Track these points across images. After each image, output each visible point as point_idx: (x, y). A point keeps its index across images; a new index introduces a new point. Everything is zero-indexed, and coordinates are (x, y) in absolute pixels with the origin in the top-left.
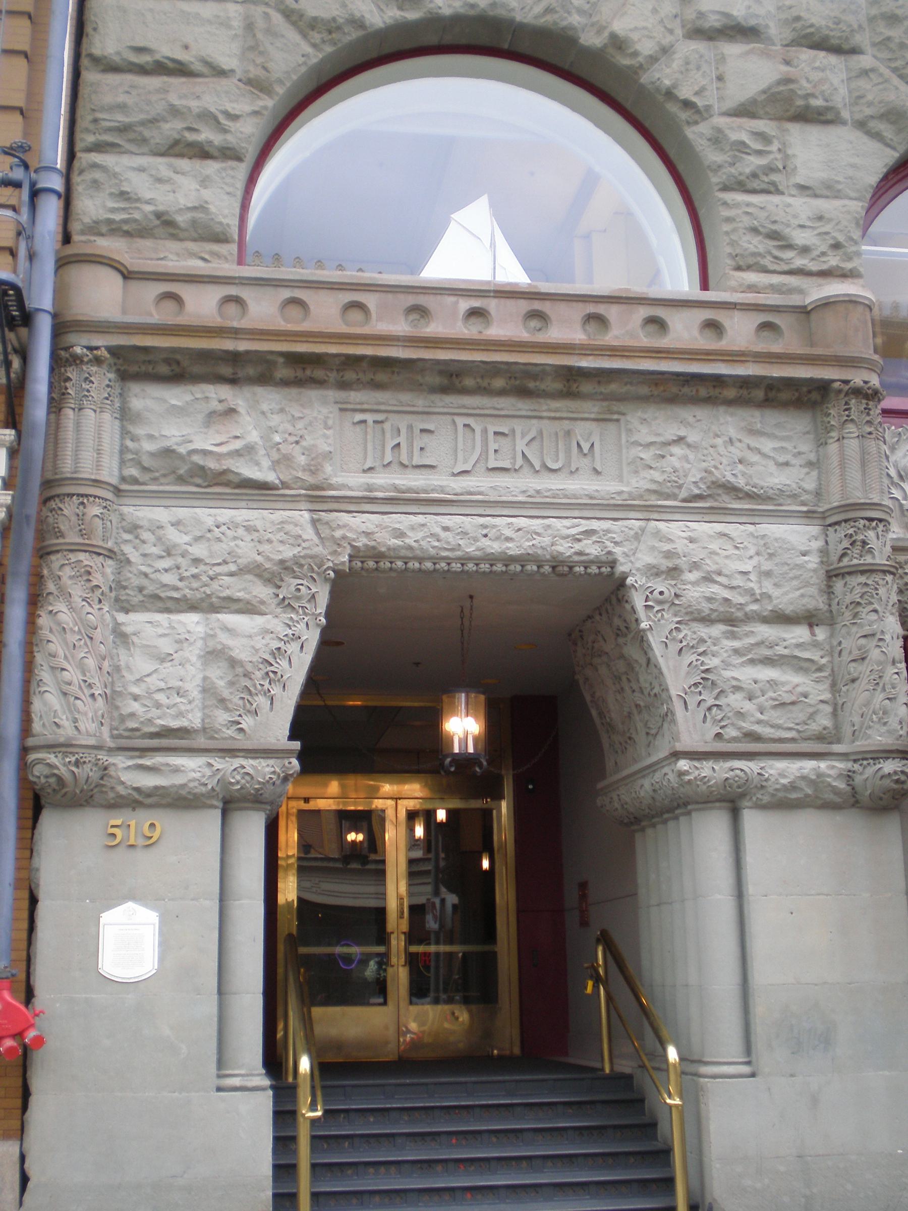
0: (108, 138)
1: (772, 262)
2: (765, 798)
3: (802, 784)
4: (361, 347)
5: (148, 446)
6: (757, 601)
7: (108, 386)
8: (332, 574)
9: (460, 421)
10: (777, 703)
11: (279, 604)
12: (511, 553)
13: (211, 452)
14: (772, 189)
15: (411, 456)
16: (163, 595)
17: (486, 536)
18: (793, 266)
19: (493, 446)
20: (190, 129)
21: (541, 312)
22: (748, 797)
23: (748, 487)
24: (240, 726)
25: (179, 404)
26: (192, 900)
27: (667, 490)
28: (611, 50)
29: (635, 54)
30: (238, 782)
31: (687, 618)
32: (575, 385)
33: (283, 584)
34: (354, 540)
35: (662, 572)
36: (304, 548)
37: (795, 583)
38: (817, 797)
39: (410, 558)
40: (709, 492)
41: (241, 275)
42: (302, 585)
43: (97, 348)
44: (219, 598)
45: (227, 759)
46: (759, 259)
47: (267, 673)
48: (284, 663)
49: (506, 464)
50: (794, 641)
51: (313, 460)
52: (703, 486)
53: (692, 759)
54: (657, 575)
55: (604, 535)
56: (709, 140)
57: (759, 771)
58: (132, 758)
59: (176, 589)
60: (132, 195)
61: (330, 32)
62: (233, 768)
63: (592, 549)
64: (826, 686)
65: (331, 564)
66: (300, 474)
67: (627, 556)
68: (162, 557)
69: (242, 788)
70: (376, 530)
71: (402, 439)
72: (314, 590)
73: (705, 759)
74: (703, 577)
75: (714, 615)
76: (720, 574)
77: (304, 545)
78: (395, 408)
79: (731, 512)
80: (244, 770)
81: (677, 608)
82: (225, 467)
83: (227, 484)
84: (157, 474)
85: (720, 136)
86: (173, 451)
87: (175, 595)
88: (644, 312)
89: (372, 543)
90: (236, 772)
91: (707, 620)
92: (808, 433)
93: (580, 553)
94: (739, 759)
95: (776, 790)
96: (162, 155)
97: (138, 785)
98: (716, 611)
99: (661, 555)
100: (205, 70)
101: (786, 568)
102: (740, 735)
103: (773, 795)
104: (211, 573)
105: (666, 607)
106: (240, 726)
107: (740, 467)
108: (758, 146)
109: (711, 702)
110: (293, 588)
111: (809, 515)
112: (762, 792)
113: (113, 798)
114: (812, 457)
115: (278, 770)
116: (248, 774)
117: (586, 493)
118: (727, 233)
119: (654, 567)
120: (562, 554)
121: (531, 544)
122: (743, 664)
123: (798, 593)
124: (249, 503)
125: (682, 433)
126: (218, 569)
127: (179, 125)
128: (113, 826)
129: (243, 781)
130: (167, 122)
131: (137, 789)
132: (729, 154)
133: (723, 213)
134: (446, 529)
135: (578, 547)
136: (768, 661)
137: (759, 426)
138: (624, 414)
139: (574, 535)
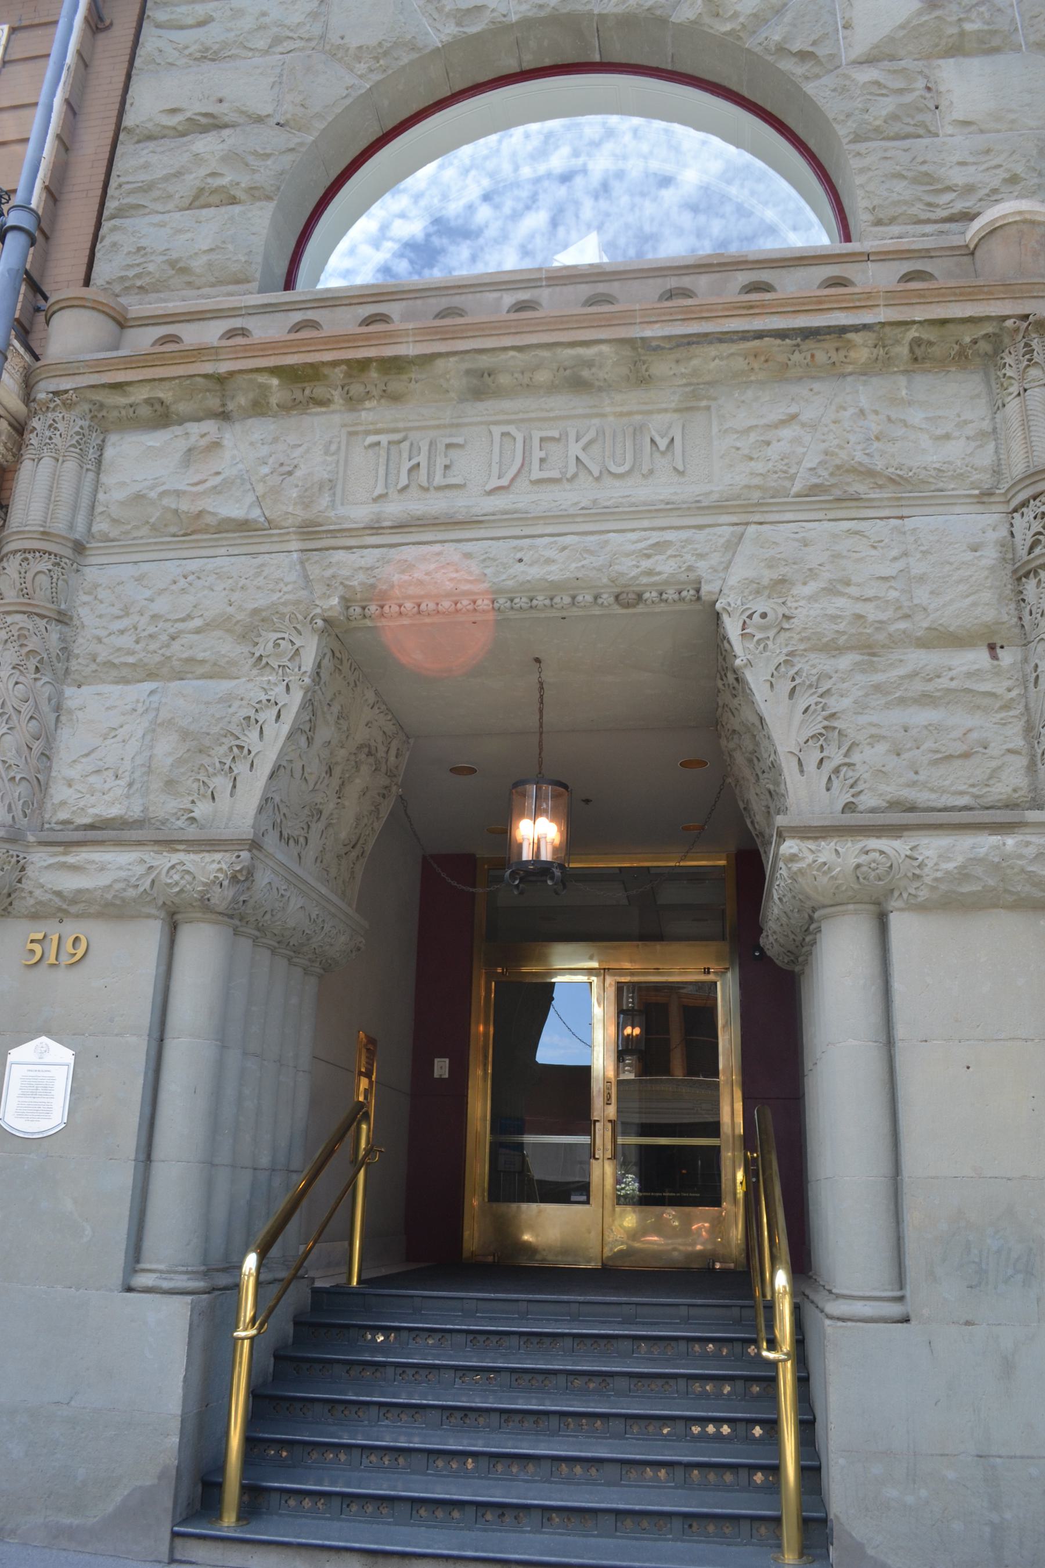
0: (131, 200)
1: (923, 210)
2: (921, 893)
3: (979, 871)
4: (362, 349)
5: (119, 495)
6: (907, 616)
7: (78, 433)
8: (320, 623)
9: (497, 430)
10: (940, 756)
11: (255, 665)
12: (551, 578)
13: (184, 492)
14: (921, 131)
15: (430, 476)
16: (116, 661)
17: (521, 560)
18: (954, 211)
19: (537, 454)
20: (213, 174)
21: (608, 295)
22: (896, 894)
23: (890, 470)
24: (192, 815)
25: (158, 444)
26: (117, 1035)
27: (773, 484)
28: (707, 20)
29: (736, 15)
30: (177, 884)
31: (802, 647)
32: (644, 367)
33: (260, 640)
34: (347, 579)
35: (765, 587)
36: (286, 593)
37: (962, 588)
38: (1006, 891)
39: (422, 597)
40: (833, 481)
41: (248, 304)
42: (283, 639)
43: (66, 392)
44: (180, 660)
45: (165, 854)
46: (904, 208)
47: (231, 749)
48: (254, 734)
49: (555, 474)
50: (965, 669)
51: (306, 490)
52: (825, 474)
53: (803, 838)
54: (758, 592)
55: (683, 547)
56: (834, 90)
57: (909, 853)
58: (55, 855)
59: (132, 653)
60: (148, 250)
61: (377, 59)
62: (170, 865)
63: (666, 567)
64: (1018, 727)
65: (318, 611)
66: (290, 509)
67: (716, 571)
68: (118, 617)
69: (182, 891)
70: (377, 564)
71: (422, 459)
72: (298, 644)
73: (824, 838)
74: (823, 589)
75: (841, 641)
76: (848, 583)
77: (285, 589)
78: (417, 424)
79: (867, 504)
80: (184, 868)
81: (788, 634)
82: (200, 509)
83: (206, 530)
84: (129, 527)
85: (847, 83)
86: (143, 496)
87: (131, 660)
88: (744, 278)
89: (372, 581)
90: (174, 871)
91: (832, 648)
92: (978, 396)
93: (650, 573)
94: (878, 837)
95: (936, 879)
96: (188, 209)
97: (59, 888)
98: (844, 633)
99: (762, 564)
100: (241, 120)
101: (948, 568)
102: (885, 804)
103: (933, 888)
104: (172, 630)
105: (771, 634)
106: (192, 815)
107: (876, 444)
108: (900, 84)
109: (838, 759)
110: (271, 644)
111: (985, 497)
112: (916, 884)
113: (32, 906)
114: (986, 425)
115: (224, 867)
116: (188, 872)
117: (661, 497)
118: (862, 186)
119: (752, 582)
120: (623, 574)
121: (580, 564)
122: (888, 706)
123: (968, 601)
124: (230, 549)
125: (793, 409)
126: (180, 626)
127: (203, 172)
128: (32, 941)
129: (183, 882)
130: (191, 173)
131: (58, 894)
132: (859, 100)
133: (854, 167)
134: (468, 556)
135: (646, 564)
136: (926, 700)
137: (904, 392)
138: (715, 399)
139: (641, 550)
